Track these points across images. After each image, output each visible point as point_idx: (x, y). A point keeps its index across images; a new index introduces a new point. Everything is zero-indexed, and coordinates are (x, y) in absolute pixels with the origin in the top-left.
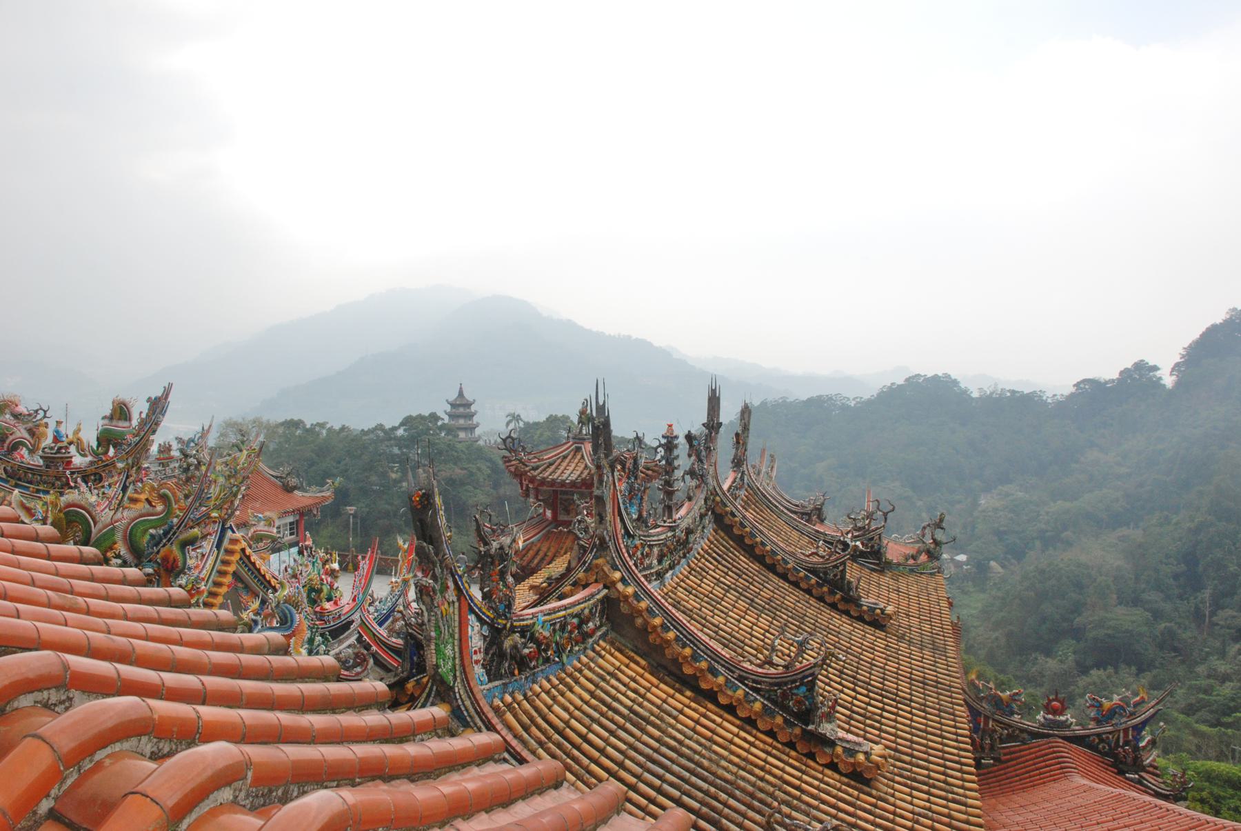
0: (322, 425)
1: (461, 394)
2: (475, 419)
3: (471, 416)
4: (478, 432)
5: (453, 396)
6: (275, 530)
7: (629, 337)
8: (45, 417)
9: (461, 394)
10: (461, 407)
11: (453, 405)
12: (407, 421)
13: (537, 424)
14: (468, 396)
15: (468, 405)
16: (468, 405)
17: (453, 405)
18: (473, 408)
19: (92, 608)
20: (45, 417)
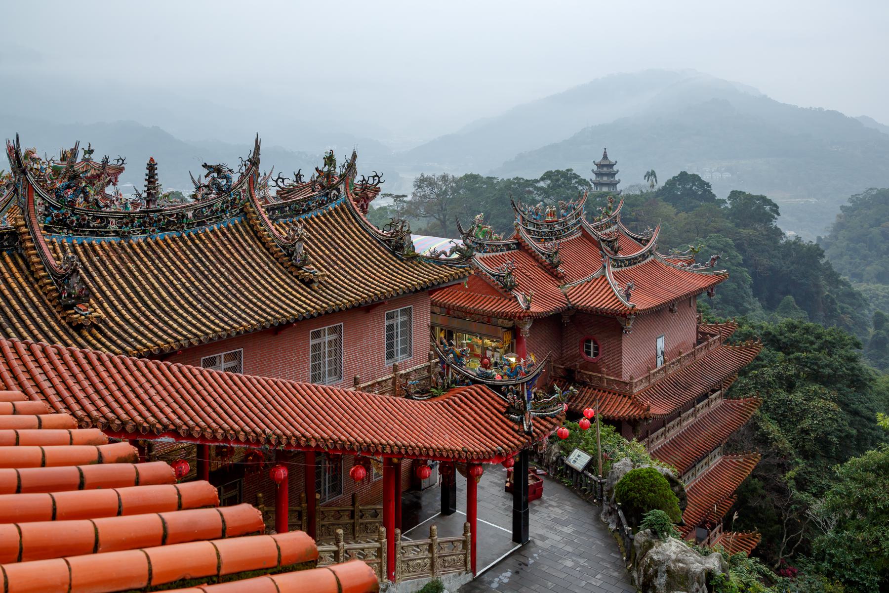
0: (495, 178)
1: (605, 157)
2: (617, 177)
3: (613, 175)
4: (619, 187)
5: (599, 159)
6: (858, 517)
7: (820, 109)
8: (379, 182)
9: (605, 157)
10: (606, 169)
11: (599, 166)
12: (548, 175)
13: (461, 178)
14: (612, 159)
15: (611, 166)
16: (611, 166)
17: (599, 166)
18: (615, 168)
19: (230, 524)
20: (379, 182)
